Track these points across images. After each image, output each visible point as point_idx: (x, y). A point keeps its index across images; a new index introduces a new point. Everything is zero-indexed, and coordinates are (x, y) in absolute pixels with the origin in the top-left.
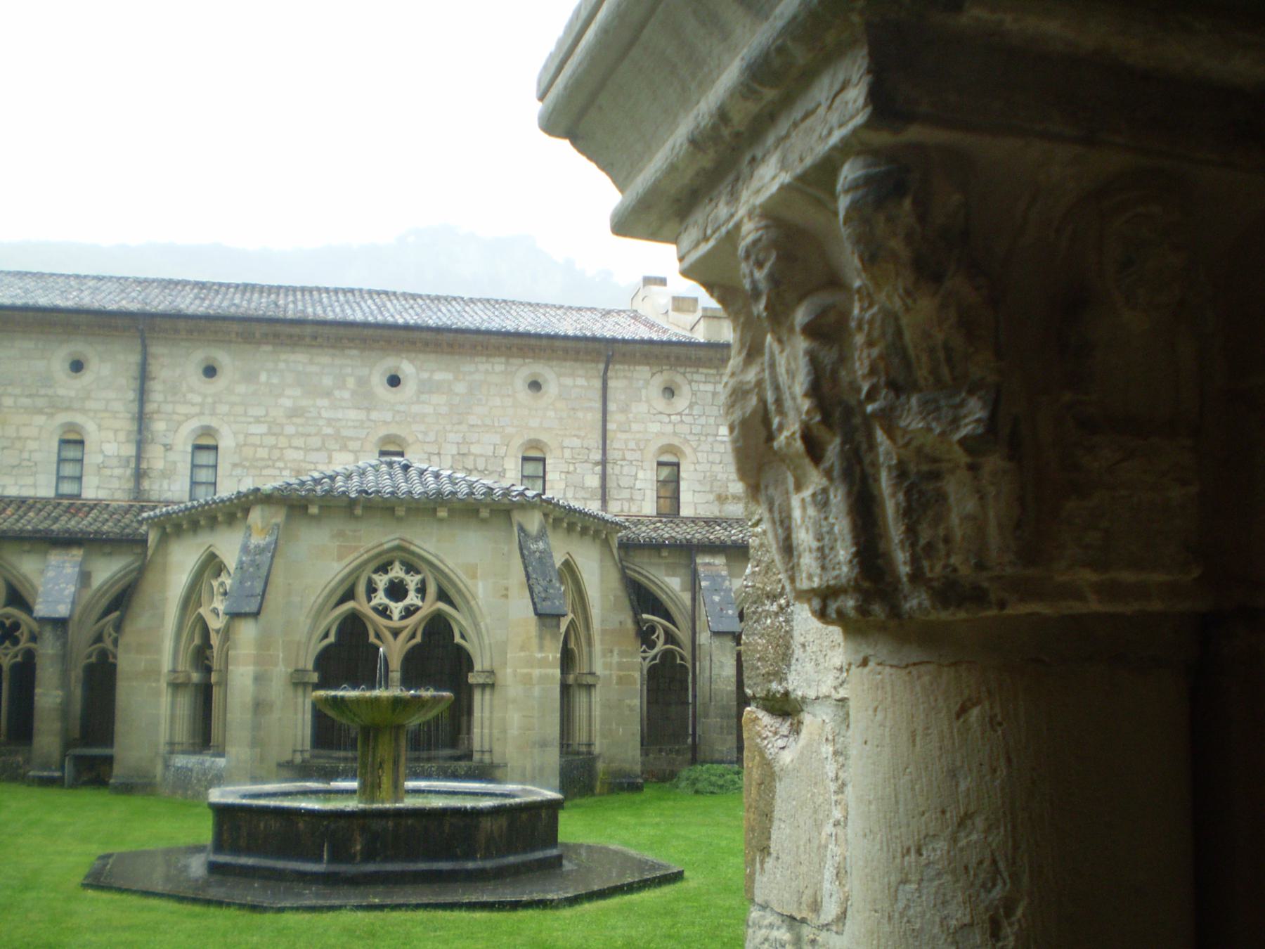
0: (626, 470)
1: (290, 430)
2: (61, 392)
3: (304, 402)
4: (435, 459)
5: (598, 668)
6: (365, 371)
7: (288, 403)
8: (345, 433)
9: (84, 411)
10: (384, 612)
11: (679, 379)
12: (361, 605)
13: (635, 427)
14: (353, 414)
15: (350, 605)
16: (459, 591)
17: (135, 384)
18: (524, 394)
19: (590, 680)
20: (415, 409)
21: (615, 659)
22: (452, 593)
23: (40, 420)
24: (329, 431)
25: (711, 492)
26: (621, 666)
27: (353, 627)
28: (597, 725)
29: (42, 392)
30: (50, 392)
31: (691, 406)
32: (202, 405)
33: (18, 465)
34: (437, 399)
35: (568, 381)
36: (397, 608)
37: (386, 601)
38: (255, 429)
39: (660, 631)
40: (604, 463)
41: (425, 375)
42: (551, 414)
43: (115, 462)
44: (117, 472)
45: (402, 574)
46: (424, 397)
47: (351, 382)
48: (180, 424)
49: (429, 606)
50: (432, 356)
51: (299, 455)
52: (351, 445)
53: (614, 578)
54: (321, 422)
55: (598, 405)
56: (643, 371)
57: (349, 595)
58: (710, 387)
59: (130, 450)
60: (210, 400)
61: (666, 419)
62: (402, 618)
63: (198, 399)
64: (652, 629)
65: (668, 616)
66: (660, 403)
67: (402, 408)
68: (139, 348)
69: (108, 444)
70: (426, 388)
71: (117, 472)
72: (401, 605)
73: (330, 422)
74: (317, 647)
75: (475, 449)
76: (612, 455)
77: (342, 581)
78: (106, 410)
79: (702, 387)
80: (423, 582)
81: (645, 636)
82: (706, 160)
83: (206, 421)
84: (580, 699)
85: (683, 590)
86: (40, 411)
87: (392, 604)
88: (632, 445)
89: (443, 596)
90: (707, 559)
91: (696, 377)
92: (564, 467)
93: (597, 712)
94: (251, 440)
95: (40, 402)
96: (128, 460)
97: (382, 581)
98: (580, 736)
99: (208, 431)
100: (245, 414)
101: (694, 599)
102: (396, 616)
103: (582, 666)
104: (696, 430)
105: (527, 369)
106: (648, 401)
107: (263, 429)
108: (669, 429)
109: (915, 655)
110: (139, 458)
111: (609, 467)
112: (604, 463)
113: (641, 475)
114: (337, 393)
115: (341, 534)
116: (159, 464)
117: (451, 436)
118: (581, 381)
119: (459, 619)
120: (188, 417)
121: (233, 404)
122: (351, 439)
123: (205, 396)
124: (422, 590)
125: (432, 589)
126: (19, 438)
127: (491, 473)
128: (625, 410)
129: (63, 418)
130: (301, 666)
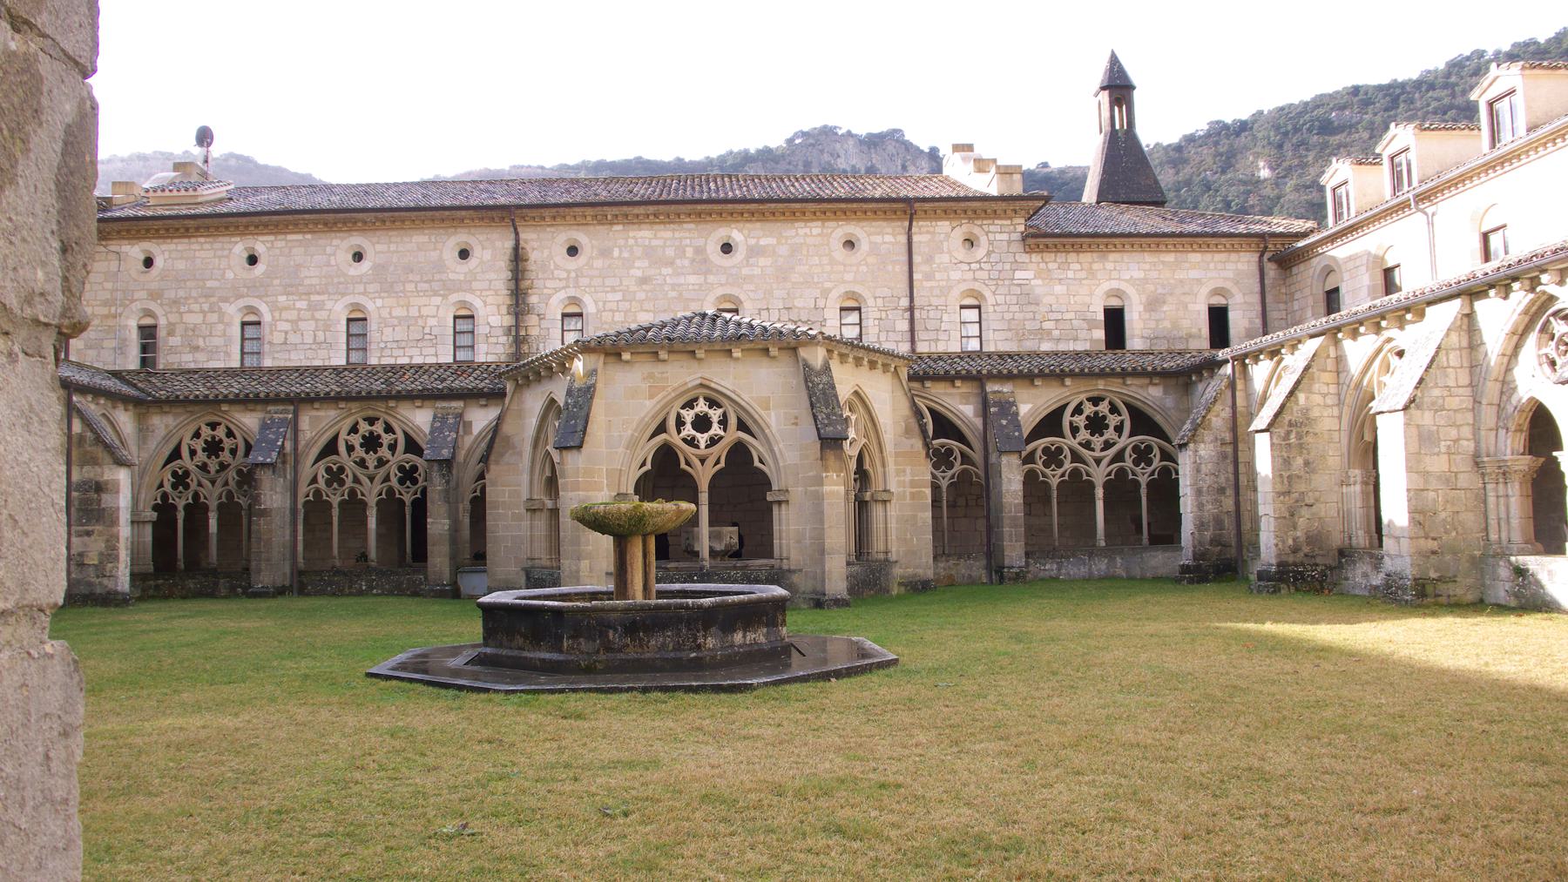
0: (932, 314)
1: (642, 296)
2: (451, 276)
4: (764, 313)
5: (893, 487)
6: (701, 242)
7: (639, 273)
8: (686, 295)
9: (471, 291)
10: (691, 442)
11: (977, 230)
12: (674, 438)
13: (938, 276)
14: (692, 279)
15: (663, 436)
16: (755, 421)
18: (840, 253)
19: (885, 496)
20: (745, 271)
21: (908, 478)
22: (749, 423)
23: (437, 300)
24: (674, 294)
26: (913, 484)
27: (666, 455)
28: (893, 536)
29: (437, 277)
30: (444, 277)
31: (989, 254)
32: (567, 279)
34: (762, 261)
35: (878, 239)
36: (702, 438)
38: (610, 297)
39: (1156, 451)
40: (911, 309)
41: (752, 242)
42: (863, 268)
43: (500, 332)
45: (706, 409)
46: (752, 261)
47: (690, 252)
48: (550, 296)
49: (733, 434)
50: (758, 225)
53: (904, 409)
55: (905, 258)
56: (944, 226)
57: (662, 428)
58: (1005, 237)
59: (508, 321)
60: (573, 275)
62: (1102, 450)
63: (564, 275)
64: (1149, 449)
65: (961, 438)
66: (961, 253)
67: (734, 271)
68: (513, 236)
69: (493, 316)
70: (754, 252)
72: (706, 435)
73: (674, 287)
74: (636, 474)
75: (798, 303)
76: (917, 302)
77: (654, 417)
79: (998, 237)
80: (724, 414)
81: (941, 459)
82: (1527, 319)
83: (572, 292)
84: (877, 512)
85: (976, 415)
86: (436, 294)
89: (742, 426)
90: (996, 388)
91: (992, 228)
92: (877, 315)
93: (893, 525)
94: (609, 306)
96: (509, 328)
97: (689, 416)
98: (877, 545)
99: (574, 301)
100: (604, 285)
101: (985, 424)
102: (702, 445)
103: (877, 484)
104: (994, 275)
105: (841, 230)
106: (949, 252)
107: (618, 296)
108: (970, 275)
110: (517, 326)
111: (917, 314)
112: (911, 309)
113: (945, 318)
114: (678, 262)
115: (651, 376)
116: (534, 332)
117: (777, 293)
118: (889, 238)
119: (756, 446)
120: (556, 290)
121: (591, 278)
123: (568, 272)
124: (724, 422)
125: (733, 421)
128: (929, 260)
129: (455, 297)
130: (623, 490)
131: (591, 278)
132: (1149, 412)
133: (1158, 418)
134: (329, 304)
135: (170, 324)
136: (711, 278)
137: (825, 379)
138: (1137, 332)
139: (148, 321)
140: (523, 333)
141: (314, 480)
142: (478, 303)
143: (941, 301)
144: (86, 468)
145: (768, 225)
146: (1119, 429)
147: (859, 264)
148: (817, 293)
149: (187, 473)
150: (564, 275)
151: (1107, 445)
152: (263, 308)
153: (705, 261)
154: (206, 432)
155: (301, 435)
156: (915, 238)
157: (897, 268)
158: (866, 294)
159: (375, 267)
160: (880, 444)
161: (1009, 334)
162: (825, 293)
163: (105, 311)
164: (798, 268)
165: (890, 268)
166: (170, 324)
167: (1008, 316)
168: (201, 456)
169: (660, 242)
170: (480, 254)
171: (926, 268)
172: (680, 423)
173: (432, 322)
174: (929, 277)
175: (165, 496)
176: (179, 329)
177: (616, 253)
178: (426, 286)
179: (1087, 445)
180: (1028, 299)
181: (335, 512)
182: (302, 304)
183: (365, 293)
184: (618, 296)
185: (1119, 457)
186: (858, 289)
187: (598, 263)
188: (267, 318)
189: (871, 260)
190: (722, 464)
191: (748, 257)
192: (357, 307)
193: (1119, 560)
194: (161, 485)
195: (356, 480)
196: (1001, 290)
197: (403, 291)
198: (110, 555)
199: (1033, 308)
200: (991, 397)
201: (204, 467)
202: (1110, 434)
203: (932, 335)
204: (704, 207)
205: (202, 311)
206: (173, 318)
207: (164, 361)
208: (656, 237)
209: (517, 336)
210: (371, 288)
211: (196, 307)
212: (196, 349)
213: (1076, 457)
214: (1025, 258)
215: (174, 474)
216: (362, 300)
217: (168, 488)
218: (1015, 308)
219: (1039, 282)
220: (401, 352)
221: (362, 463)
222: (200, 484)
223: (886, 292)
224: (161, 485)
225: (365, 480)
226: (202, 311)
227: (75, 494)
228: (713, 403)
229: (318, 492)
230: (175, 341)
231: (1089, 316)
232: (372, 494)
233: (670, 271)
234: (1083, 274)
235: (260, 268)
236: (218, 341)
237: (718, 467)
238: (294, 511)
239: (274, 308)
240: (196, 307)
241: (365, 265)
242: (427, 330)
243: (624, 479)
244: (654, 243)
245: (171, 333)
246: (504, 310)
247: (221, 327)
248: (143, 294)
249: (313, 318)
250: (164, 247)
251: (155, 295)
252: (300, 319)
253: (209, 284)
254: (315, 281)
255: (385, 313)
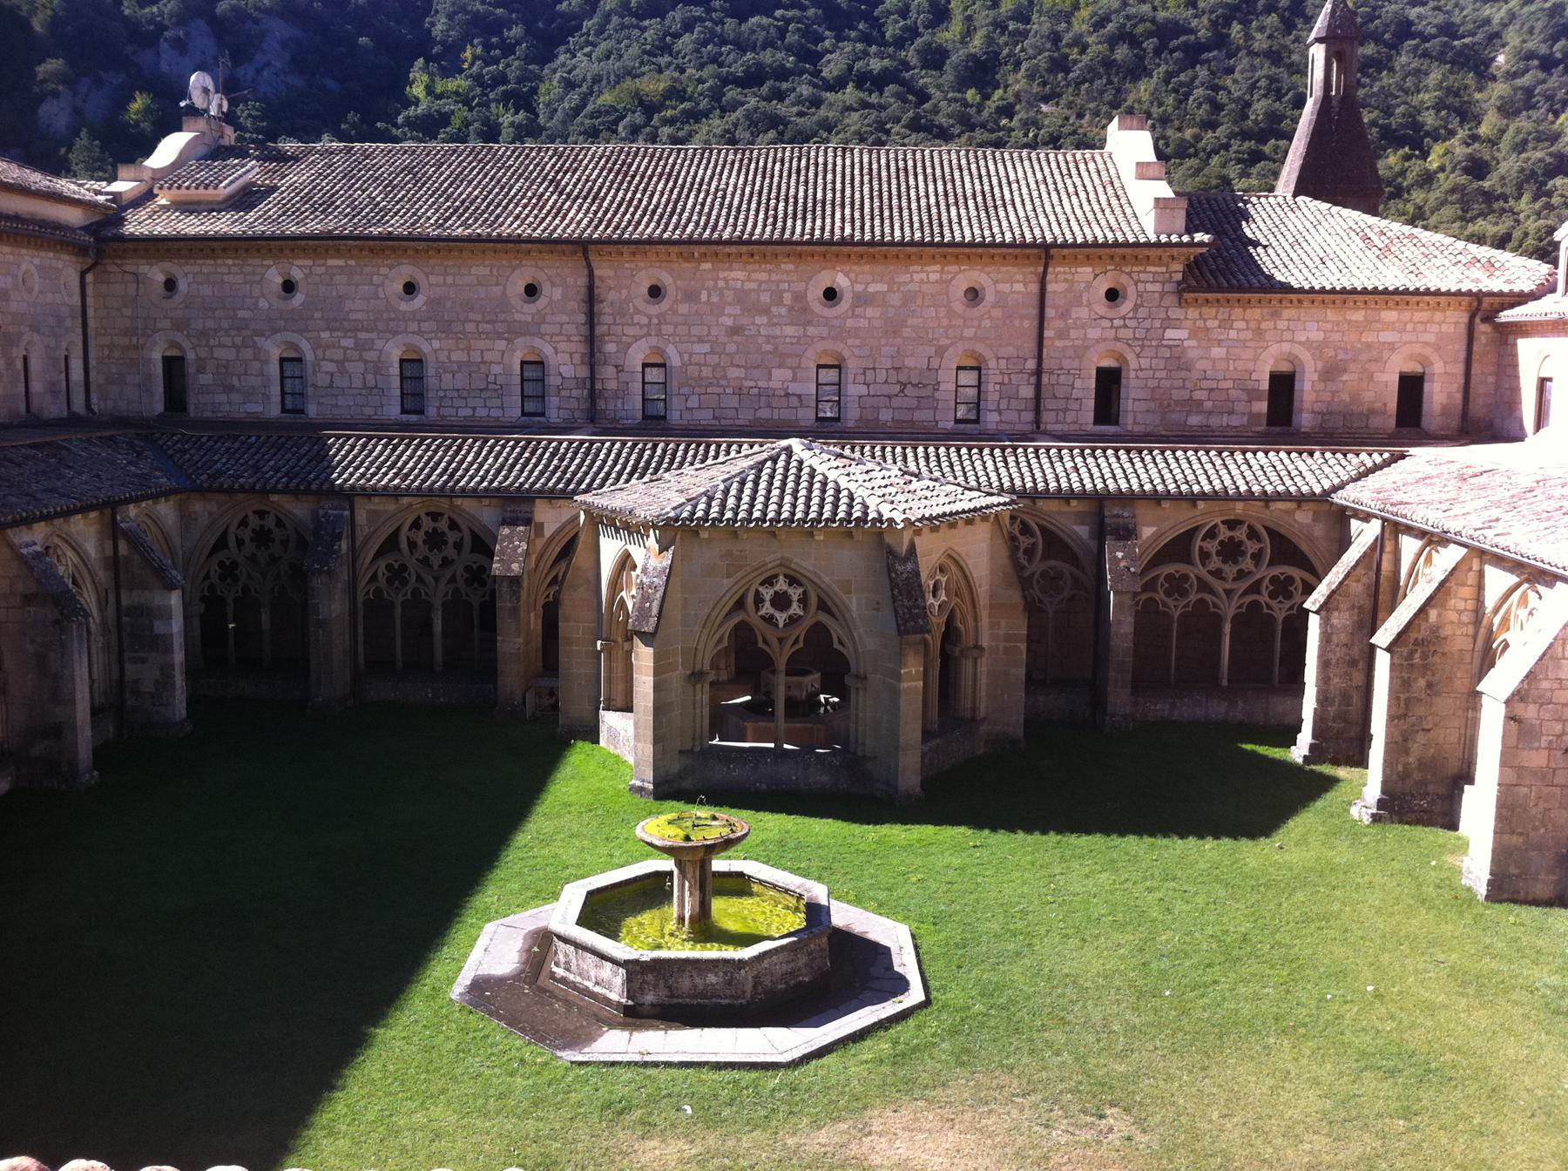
1: (731, 348)
2: (517, 317)
3: (744, 321)
4: (870, 374)
7: (729, 322)
9: (542, 336)
12: (754, 620)
13: (1073, 334)
14: (790, 330)
17: (584, 308)
20: (850, 323)
21: (1002, 632)
23: (502, 344)
24: (768, 347)
25: (1153, 400)
26: (1008, 638)
29: (502, 317)
31: (1136, 308)
32: (649, 324)
33: (487, 389)
35: (1006, 288)
37: (772, 611)
38: (697, 348)
40: (1038, 372)
41: (859, 288)
42: (987, 323)
43: (573, 384)
44: (575, 393)
45: (785, 587)
46: (858, 311)
47: (787, 297)
48: (629, 345)
51: (740, 373)
52: (789, 362)
54: (760, 340)
55: (1035, 312)
56: (1086, 271)
57: (740, 604)
58: (1157, 287)
59: (583, 372)
60: (655, 321)
61: (1107, 323)
67: (837, 323)
71: (575, 393)
73: (768, 338)
75: (909, 362)
76: (1046, 365)
78: (560, 334)
79: (1150, 287)
80: (805, 593)
85: (1091, 537)
86: (500, 337)
87: (777, 614)
88: (1070, 353)
89: (823, 606)
91: (1143, 276)
93: (983, 681)
94: (695, 359)
95: (500, 327)
97: (768, 593)
100: (690, 335)
104: (1140, 333)
106: (1089, 305)
107: (706, 348)
108: (1111, 333)
109: (960, 1087)
111: (1045, 379)
112: (1038, 372)
113: (1078, 383)
114: (774, 309)
117: (886, 350)
118: (1019, 287)
119: (835, 630)
120: (637, 338)
122: (790, 355)
123: (650, 317)
125: (813, 601)
126: (483, 362)
127: (925, 386)
128: (1064, 315)
130: (698, 667)
131: (676, 325)
132: (1294, 540)
133: (1304, 547)
134: (379, 344)
135: (199, 359)
136: (811, 330)
137: (909, 566)
138: (1307, 405)
139: (174, 353)
140: (598, 386)
141: (374, 578)
142: (548, 350)
143: (1076, 364)
144: (135, 593)
145: (880, 268)
146: (1257, 557)
147: (981, 318)
148: (931, 351)
149: (235, 565)
150: (646, 321)
151: (1241, 575)
152: (305, 346)
153: (806, 310)
154: (254, 521)
155: (358, 529)
156: (1050, 288)
157: (1026, 323)
158: (988, 354)
159: (429, 302)
160: (973, 599)
161: (1152, 405)
162: (941, 351)
163: (124, 341)
164: (910, 321)
165: (1017, 323)
166: (199, 359)
167: (1152, 383)
168: (249, 548)
169: (754, 286)
170: (552, 293)
171: (1059, 324)
172: (759, 600)
173: (496, 369)
174: (1062, 335)
175: (212, 587)
176: (210, 366)
177: (704, 296)
178: (488, 327)
179: (1218, 574)
180: (1178, 361)
181: (398, 611)
182: (348, 342)
183: (419, 332)
184: (706, 348)
185: (1255, 588)
186: (980, 348)
187: (684, 308)
188: (309, 356)
189: (997, 313)
190: (801, 645)
191: (853, 307)
192: (412, 348)
193: (1240, 704)
194: (207, 577)
195: (419, 579)
196: (1147, 352)
197: (463, 332)
198: (165, 682)
199: (1183, 374)
200: (1107, 520)
201: (252, 559)
202: (1247, 563)
203: (1061, 404)
204: (805, 248)
205: (234, 345)
206: (203, 353)
207: (197, 404)
208: (749, 280)
209: (592, 389)
210: (426, 326)
211: (227, 341)
212: (229, 389)
213: (1204, 586)
214: (1177, 313)
215: (221, 564)
216: (417, 340)
217: (215, 578)
218: (1163, 374)
219: (1194, 343)
220: (462, 403)
221: (425, 562)
222: (249, 577)
223: (1011, 352)
224: (207, 577)
225: (429, 579)
226: (234, 345)
227: (126, 619)
228: (793, 581)
229: (378, 591)
230: (206, 379)
231: (1250, 385)
232: (439, 594)
233: (764, 320)
234: (1249, 334)
235: (298, 299)
236: (254, 381)
237: (797, 647)
238: (353, 612)
239: (317, 345)
240: (227, 341)
241: (419, 301)
242: (491, 379)
243: (699, 656)
244: (748, 286)
245: (201, 370)
246: (577, 358)
247: (257, 365)
248: (166, 324)
249: (361, 359)
250: (187, 268)
251: (180, 325)
252: (346, 359)
253: (241, 314)
254: (360, 316)
255: (443, 357)
